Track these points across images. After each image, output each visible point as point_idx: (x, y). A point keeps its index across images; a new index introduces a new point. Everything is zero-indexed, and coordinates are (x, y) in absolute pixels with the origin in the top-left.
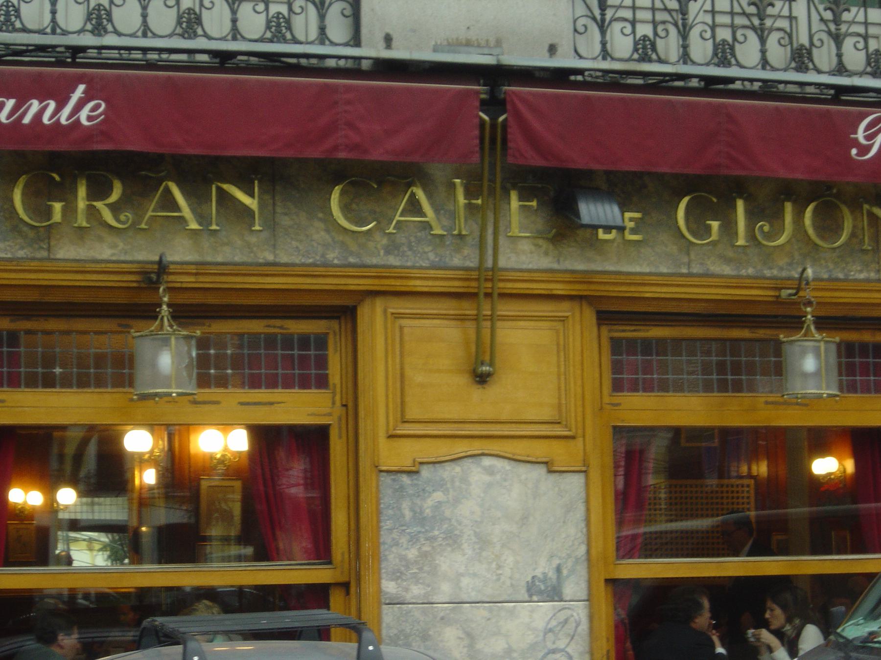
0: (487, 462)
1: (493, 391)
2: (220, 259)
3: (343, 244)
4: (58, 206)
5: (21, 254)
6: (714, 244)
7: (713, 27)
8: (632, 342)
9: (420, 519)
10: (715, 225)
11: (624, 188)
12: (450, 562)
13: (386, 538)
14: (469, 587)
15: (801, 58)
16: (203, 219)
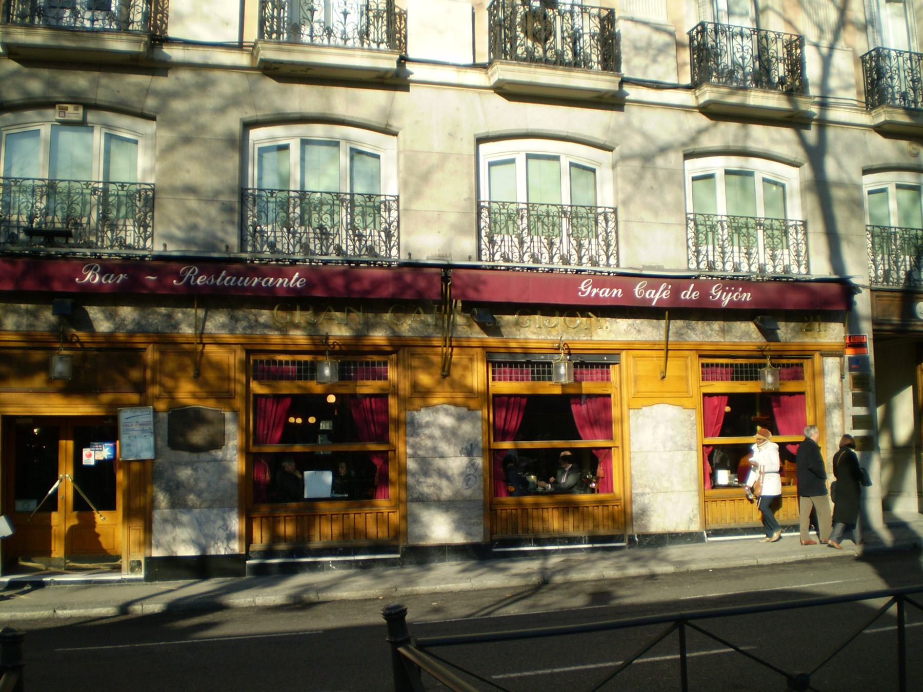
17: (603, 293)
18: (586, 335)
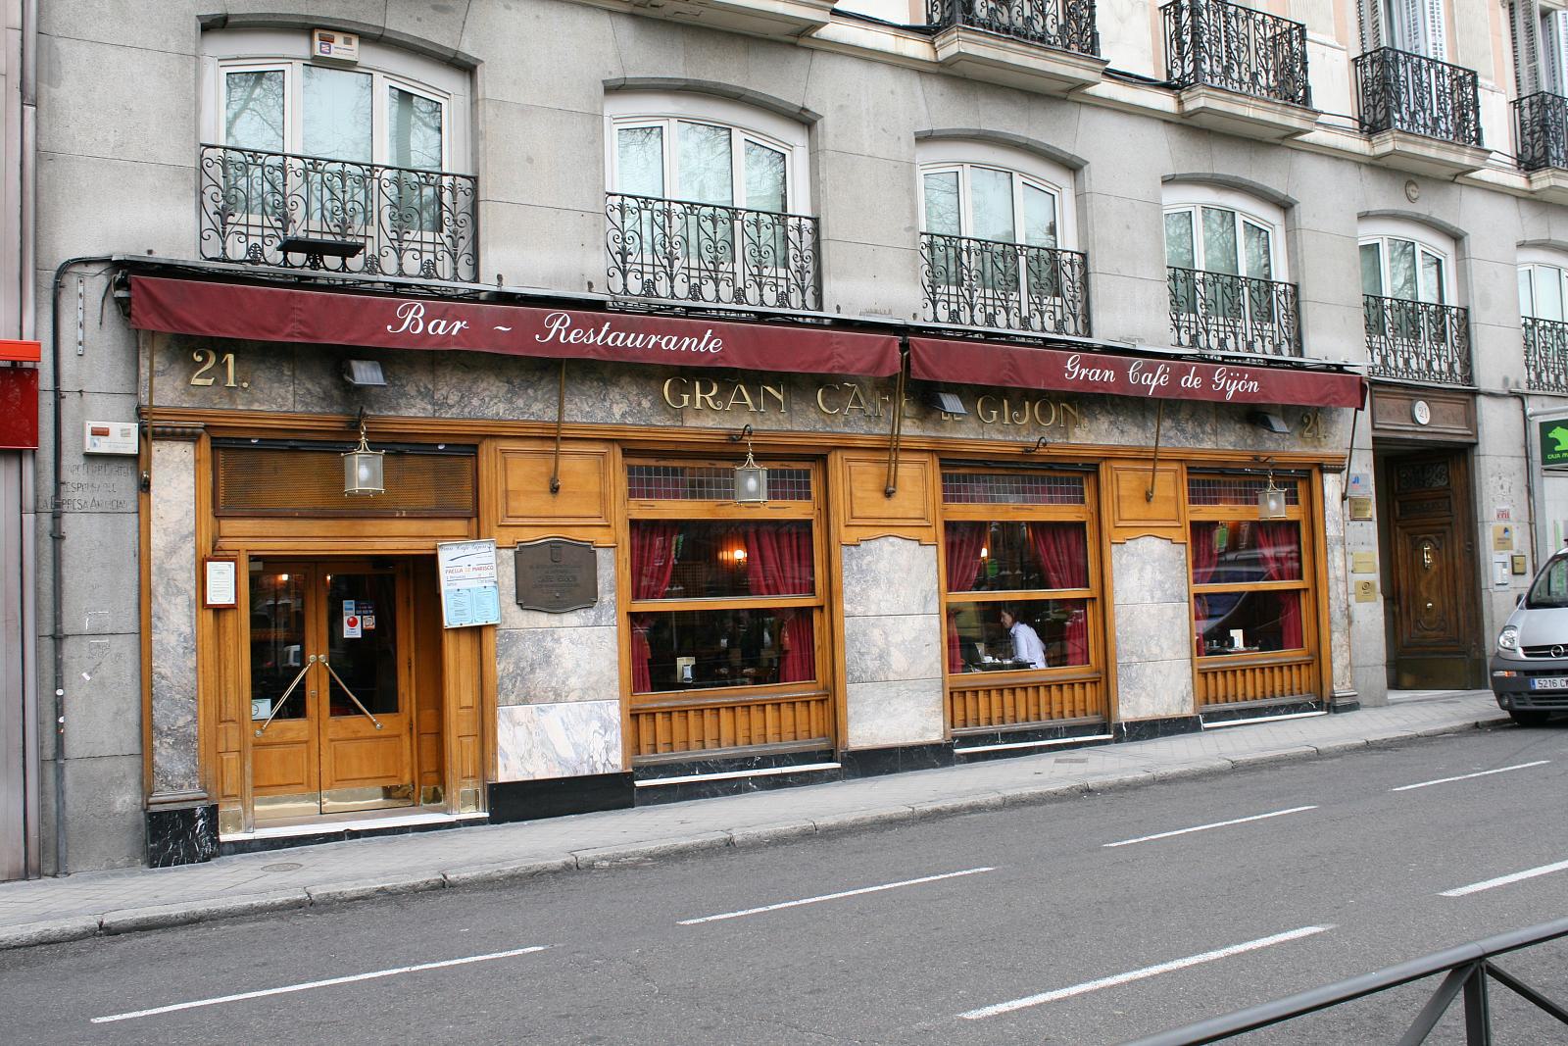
0: (891, 539)
1: (895, 500)
2: (765, 428)
3: (824, 421)
4: (686, 397)
5: (668, 423)
6: (994, 423)
7: (689, 277)
8: (951, 475)
9: (861, 571)
10: (995, 412)
11: (970, 393)
12: (875, 594)
13: (845, 581)
14: (885, 608)
15: (1025, 323)
16: (757, 405)
17: (668, 344)
18: (1062, 436)
